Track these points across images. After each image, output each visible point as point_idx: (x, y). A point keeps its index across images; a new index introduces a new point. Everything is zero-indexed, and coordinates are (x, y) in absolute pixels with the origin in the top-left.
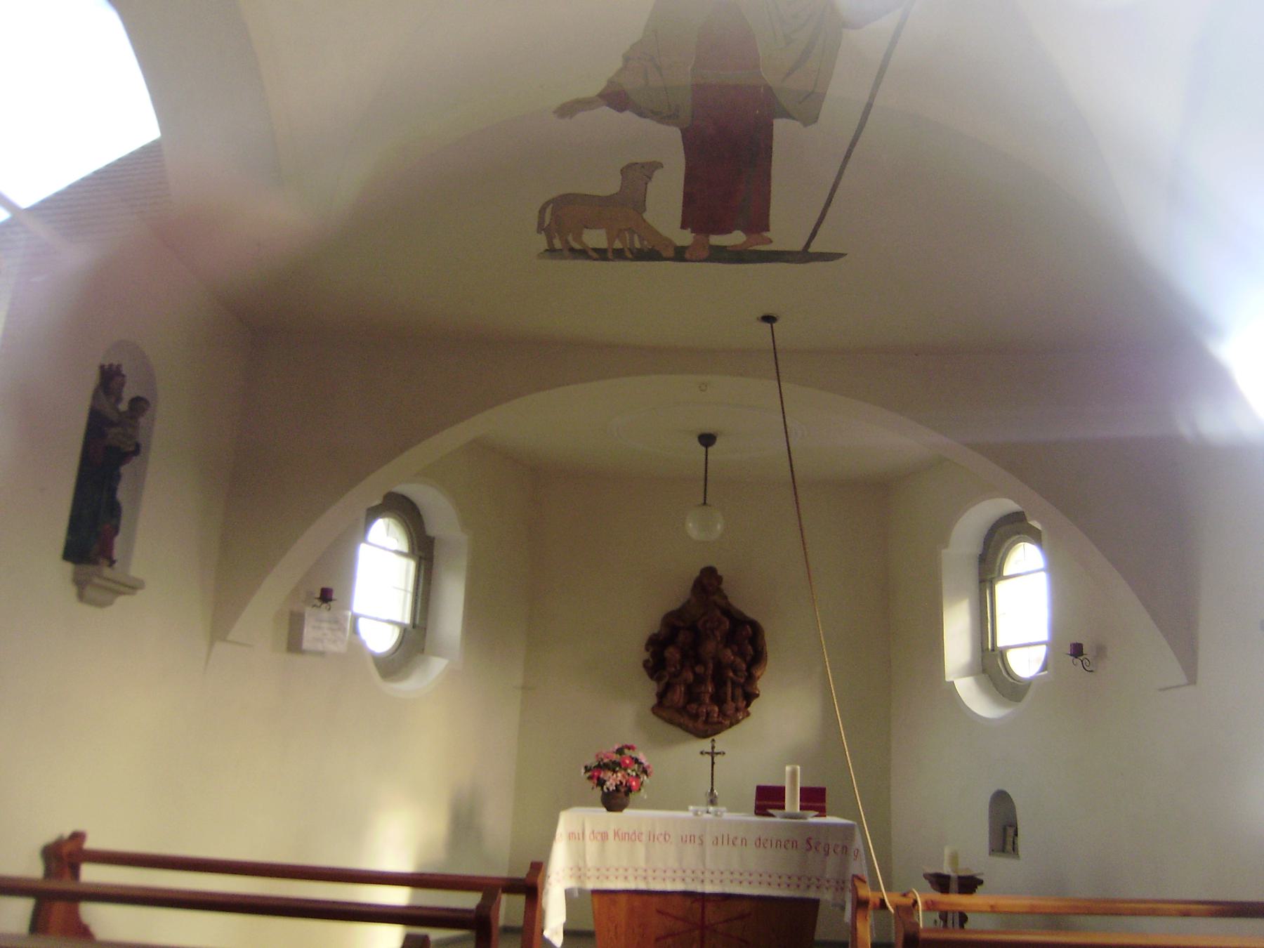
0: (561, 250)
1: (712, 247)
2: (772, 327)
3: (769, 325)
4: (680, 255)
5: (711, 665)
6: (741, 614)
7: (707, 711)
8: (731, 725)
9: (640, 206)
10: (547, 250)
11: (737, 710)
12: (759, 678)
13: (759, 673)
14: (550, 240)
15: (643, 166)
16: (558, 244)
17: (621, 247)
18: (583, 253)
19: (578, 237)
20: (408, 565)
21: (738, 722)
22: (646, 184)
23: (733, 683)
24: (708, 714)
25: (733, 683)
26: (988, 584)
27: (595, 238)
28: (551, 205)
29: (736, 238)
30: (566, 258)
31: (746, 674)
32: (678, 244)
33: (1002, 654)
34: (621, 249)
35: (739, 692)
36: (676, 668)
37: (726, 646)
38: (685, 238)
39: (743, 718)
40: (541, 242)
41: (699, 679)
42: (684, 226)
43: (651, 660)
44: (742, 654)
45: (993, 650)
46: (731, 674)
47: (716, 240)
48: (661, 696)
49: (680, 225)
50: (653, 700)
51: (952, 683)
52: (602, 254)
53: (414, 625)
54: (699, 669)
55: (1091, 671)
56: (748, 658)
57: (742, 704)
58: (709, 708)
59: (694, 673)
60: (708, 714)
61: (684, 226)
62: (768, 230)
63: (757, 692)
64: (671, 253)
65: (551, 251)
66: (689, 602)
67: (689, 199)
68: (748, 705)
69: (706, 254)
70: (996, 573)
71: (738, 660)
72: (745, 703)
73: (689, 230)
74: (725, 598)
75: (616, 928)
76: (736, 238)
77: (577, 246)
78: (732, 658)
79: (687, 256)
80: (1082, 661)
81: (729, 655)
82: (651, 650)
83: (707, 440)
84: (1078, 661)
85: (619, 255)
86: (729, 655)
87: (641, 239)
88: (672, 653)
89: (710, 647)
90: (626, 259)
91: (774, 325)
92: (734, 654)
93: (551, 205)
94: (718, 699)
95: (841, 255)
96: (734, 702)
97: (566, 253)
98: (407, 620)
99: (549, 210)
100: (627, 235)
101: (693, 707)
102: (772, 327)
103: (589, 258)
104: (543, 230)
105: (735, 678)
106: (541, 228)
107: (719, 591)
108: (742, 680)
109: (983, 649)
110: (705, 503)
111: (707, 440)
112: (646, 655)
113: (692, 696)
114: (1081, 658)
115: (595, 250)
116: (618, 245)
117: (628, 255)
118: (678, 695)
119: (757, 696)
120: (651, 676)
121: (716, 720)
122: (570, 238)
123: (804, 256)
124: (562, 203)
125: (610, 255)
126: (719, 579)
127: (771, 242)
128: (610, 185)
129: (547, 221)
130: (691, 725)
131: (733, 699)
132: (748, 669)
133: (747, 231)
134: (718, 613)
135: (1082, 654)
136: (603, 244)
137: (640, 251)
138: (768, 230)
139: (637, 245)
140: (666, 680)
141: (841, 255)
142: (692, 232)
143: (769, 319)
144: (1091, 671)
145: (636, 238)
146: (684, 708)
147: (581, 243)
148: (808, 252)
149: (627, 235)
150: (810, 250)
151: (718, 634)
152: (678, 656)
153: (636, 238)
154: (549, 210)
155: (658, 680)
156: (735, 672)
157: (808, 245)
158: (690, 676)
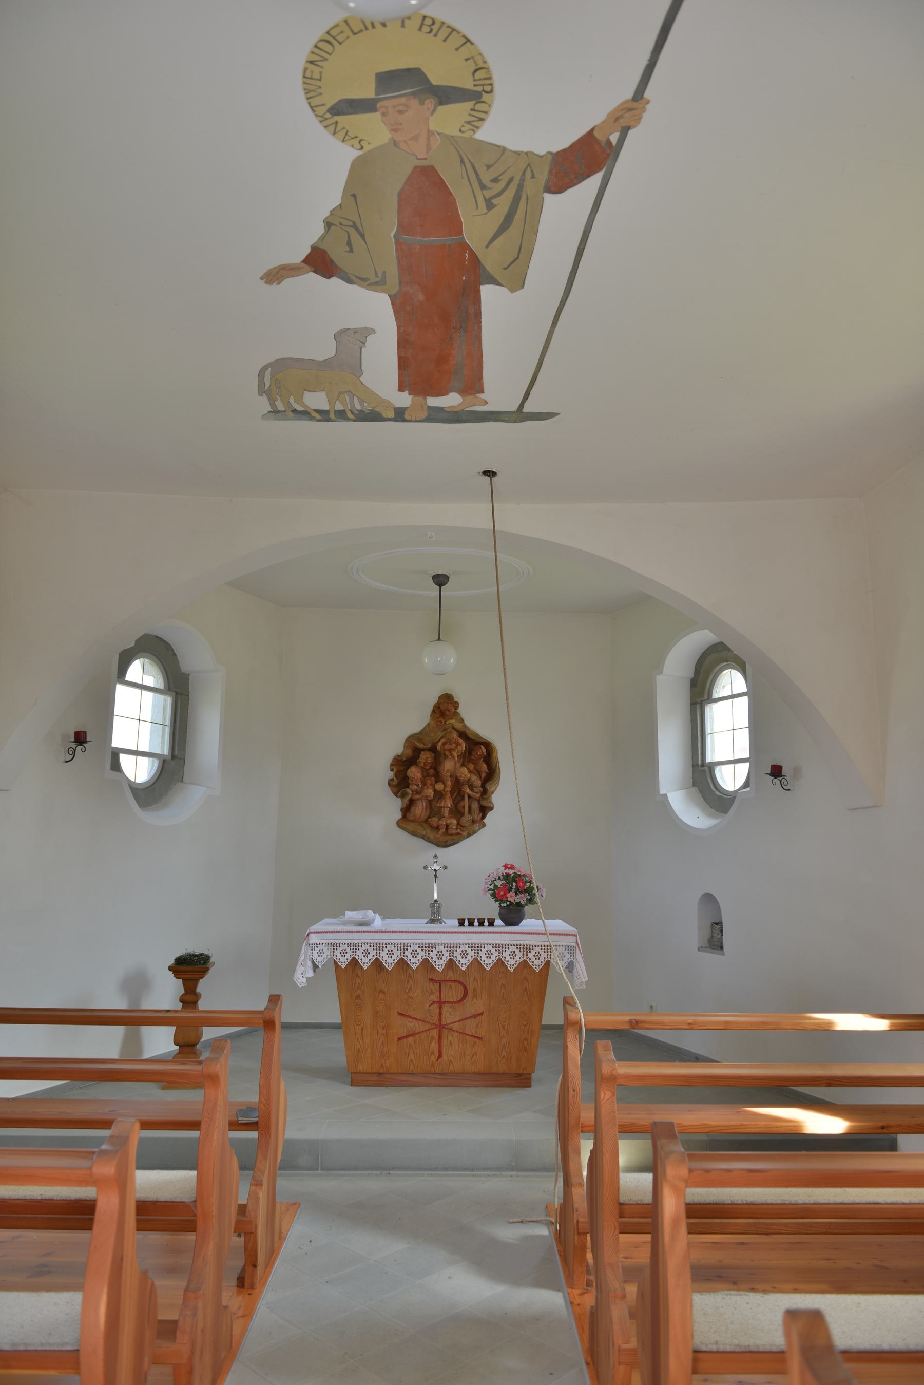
0: (285, 411)
1: (429, 408)
2: (491, 480)
3: (489, 478)
4: (400, 415)
5: (449, 783)
6: (477, 735)
7: (446, 824)
8: (469, 835)
9: (357, 370)
10: (270, 412)
11: (474, 822)
12: (493, 793)
13: (493, 789)
14: (272, 402)
15: (356, 331)
16: (280, 406)
17: (343, 409)
18: (305, 414)
19: (299, 399)
20: (165, 701)
21: (474, 832)
22: (361, 348)
23: (469, 797)
24: (447, 826)
25: (469, 797)
26: (698, 706)
27: (316, 400)
28: (270, 369)
29: (452, 400)
30: (288, 419)
31: (482, 790)
32: (397, 406)
33: (712, 767)
34: (343, 410)
35: (475, 805)
36: (417, 786)
37: (462, 765)
38: (404, 400)
39: (479, 829)
40: (264, 405)
41: (439, 795)
42: (401, 389)
43: (395, 779)
44: (479, 773)
45: (703, 765)
46: (468, 790)
47: (433, 401)
48: (406, 811)
49: (397, 388)
50: (399, 815)
51: (665, 795)
52: (324, 415)
53: (173, 757)
54: (439, 786)
55: (789, 790)
56: (483, 775)
57: (477, 815)
58: (448, 821)
59: (435, 791)
60: (447, 826)
61: (401, 389)
62: (483, 392)
63: (492, 806)
64: (391, 414)
65: (275, 412)
66: (429, 725)
67: (403, 364)
68: (484, 817)
69: (424, 415)
70: (706, 697)
71: (474, 778)
72: (481, 815)
73: (407, 392)
74: (462, 721)
75: (362, 1030)
76: (452, 400)
77: (299, 408)
78: (469, 775)
79: (407, 416)
80: (781, 781)
81: (464, 773)
82: (395, 770)
83: (441, 580)
84: (777, 781)
85: (341, 415)
86: (464, 773)
87: (361, 401)
88: (414, 773)
89: (448, 766)
90: (348, 419)
91: (493, 478)
92: (470, 772)
93: (270, 369)
94: (457, 812)
95: (557, 414)
96: (471, 815)
97: (291, 414)
98: (166, 752)
99: (268, 374)
100: (347, 398)
101: (434, 821)
102: (491, 480)
103: (312, 418)
104: (265, 392)
105: (470, 793)
106: (261, 391)
107: (456, 714)
108: (478, 796)
109: (695, 766)
110: (439, 639)
111: (441, 580)
112: (391, 775)
113: (433, 810)
114: (780, 779)
115: (317, 411)
116: (339, 407)
117: (350, 415)
118: (420, 810)
119: (491, 809)
120: (396, 794)
121: (455, 832)
122: (292, 400)
123: (520, 415)
124: (280, 366)
125: (332, 416)
126: (456, 705)
127: (486, 403)
128: (326, 350)
129: (267, 384)
130: (432, 837)
131: (470, 812)
132: (483, 786)
133: (463, 392)
134: (455, 735)
135: (780, 775)
136: (325, 407)
137: (361, 411)
138: (483, 392)
139: (358, 407)
140: (408, 797)
141: (557, 414)
142: (409, 394)
143: (490, 474)
144: (789, 790)
145: (356, 400)
146: (426, 821)
147: (303, 405)
148: (523, 412)
149: (347, 398)
150: (525, 410)
151: (455, 754)
152: (419, 775)
153: (356, 400)
154: (268, 374)
155: (403, 796)
156: (472, 789)
157: (522, 405)
158: (430, 792)
